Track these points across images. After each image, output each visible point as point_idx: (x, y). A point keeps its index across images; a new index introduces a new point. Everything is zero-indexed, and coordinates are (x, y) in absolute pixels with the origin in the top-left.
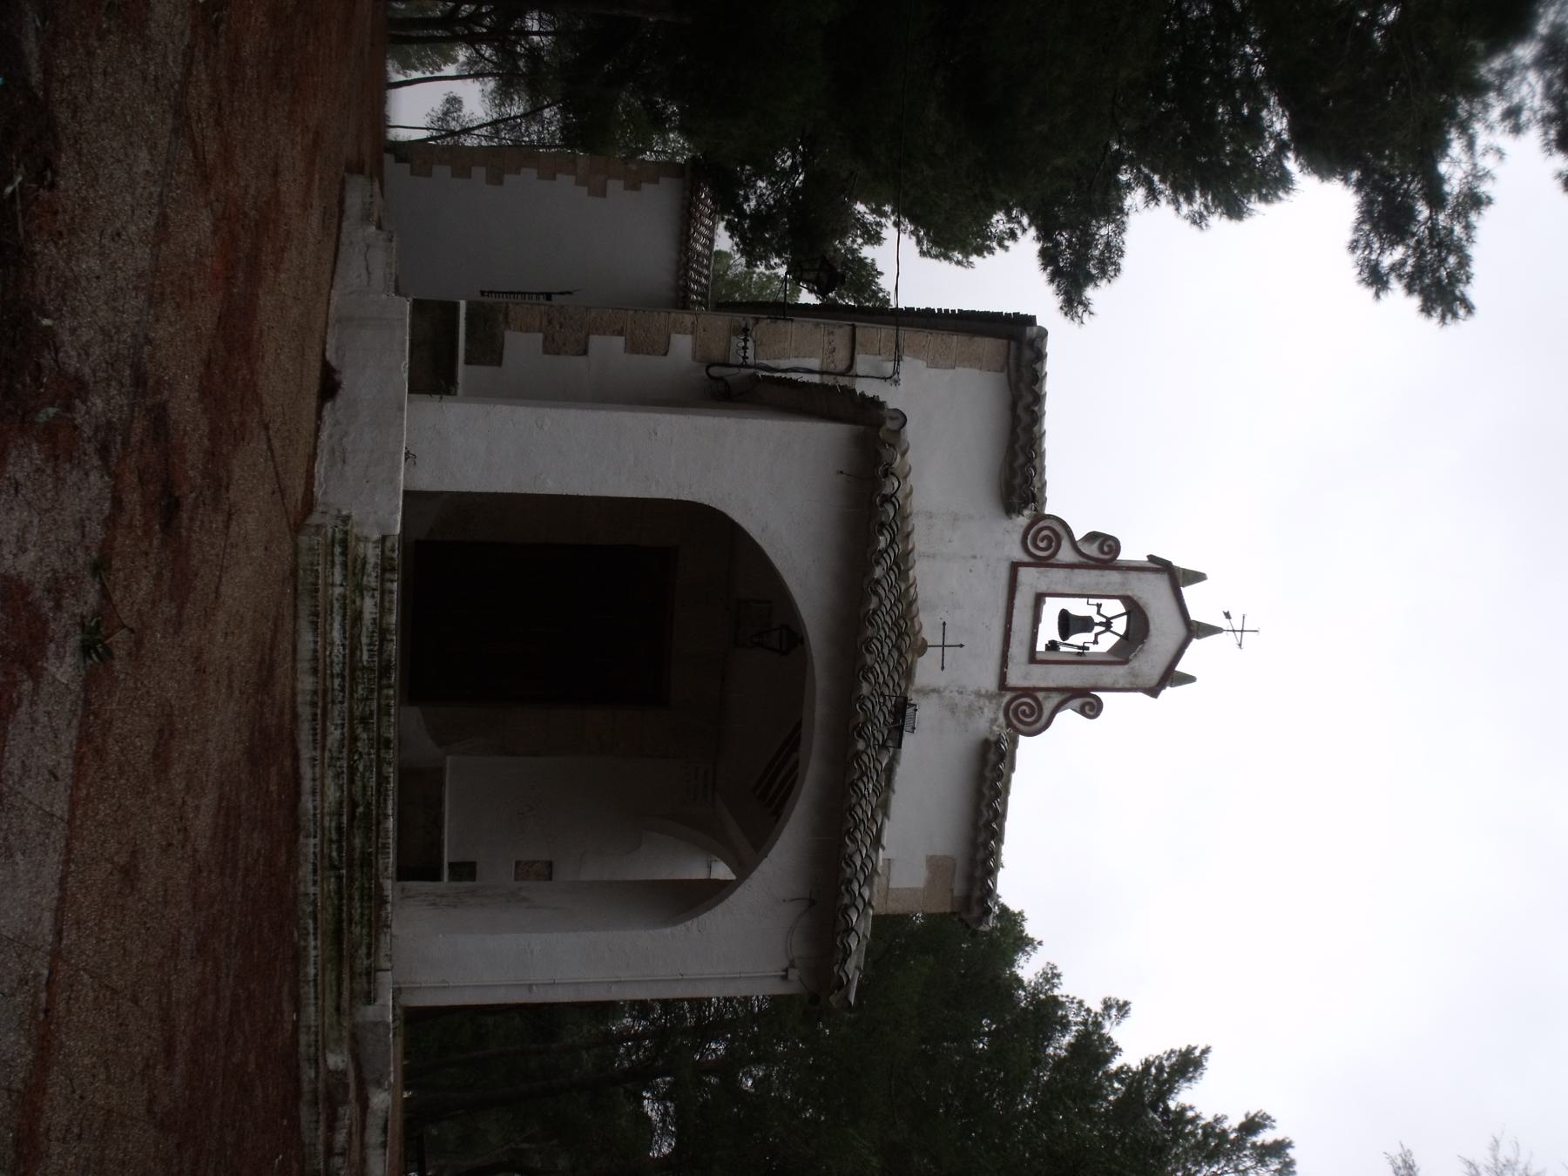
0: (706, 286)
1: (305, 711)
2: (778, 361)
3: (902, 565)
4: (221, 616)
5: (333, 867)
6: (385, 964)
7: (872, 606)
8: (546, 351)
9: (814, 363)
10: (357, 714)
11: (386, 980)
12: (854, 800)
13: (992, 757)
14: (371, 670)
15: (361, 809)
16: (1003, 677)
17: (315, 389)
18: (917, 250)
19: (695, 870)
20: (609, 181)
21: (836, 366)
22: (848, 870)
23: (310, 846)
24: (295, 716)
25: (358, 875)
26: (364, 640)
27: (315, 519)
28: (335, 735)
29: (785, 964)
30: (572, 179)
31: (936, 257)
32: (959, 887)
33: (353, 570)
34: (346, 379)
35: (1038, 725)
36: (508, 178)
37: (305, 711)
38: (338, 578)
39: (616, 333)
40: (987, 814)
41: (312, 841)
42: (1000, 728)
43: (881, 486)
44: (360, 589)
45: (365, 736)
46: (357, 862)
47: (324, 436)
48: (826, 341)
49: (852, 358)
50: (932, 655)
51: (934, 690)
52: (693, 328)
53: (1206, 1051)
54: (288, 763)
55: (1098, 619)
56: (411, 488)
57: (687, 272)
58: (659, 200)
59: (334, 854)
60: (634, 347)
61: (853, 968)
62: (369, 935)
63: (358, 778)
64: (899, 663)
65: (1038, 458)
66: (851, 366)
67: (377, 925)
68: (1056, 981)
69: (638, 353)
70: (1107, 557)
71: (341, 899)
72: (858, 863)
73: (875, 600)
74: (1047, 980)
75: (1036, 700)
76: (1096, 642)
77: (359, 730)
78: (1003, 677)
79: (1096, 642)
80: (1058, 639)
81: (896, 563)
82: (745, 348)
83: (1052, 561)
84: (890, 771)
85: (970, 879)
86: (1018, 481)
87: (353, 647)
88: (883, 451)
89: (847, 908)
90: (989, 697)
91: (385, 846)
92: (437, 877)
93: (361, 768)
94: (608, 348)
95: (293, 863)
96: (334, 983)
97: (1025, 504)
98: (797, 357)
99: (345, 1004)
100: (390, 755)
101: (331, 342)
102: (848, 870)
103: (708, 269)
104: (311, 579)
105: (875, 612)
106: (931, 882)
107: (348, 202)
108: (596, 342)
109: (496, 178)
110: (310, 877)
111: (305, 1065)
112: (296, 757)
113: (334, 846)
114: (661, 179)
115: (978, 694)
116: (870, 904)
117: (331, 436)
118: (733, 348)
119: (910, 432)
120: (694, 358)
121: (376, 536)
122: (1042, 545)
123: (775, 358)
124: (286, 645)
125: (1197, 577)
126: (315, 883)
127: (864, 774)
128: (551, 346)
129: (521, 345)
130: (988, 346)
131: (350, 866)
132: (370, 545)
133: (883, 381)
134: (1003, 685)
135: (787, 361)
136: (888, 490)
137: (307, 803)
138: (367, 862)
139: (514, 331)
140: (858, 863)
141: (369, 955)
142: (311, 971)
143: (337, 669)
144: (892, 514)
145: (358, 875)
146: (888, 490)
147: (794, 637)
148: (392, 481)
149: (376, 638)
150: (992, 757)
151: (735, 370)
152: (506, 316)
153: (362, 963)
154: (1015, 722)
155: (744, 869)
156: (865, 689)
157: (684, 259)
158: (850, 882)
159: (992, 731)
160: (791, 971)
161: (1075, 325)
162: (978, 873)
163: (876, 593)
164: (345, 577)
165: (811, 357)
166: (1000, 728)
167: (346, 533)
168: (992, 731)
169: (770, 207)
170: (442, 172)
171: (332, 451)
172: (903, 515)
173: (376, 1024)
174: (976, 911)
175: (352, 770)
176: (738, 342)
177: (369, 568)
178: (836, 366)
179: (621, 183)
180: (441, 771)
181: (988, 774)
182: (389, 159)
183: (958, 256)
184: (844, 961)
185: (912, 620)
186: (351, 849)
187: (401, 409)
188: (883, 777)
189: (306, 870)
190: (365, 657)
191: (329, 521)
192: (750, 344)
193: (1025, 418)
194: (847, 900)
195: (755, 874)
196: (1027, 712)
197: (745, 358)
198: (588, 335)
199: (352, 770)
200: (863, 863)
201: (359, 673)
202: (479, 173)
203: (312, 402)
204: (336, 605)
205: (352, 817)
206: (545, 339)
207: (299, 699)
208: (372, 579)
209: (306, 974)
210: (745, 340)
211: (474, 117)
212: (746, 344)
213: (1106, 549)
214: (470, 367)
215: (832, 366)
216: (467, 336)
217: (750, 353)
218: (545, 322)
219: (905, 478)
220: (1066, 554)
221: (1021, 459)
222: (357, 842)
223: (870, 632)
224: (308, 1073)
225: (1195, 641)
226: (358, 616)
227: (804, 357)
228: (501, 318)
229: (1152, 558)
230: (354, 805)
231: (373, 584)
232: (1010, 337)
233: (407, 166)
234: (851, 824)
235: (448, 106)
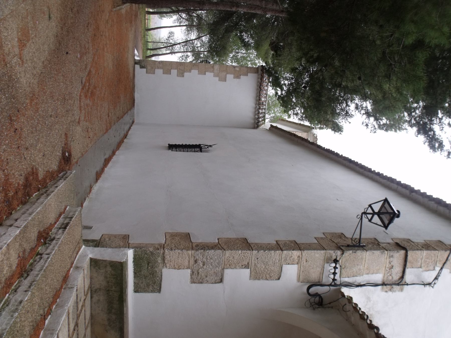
2: (355, 278)
20: (227, 75)
21: (392, 278)
30: (212, 74)
36: (186, 74)
39: (244, 267)
48: (388, 263)
49: (404, 272)
52: (299, 260)
60: (255, 276)
66: (402, 277)
69: (259, 279)
82: (334, 274)
98: (368, 274)
108: (229, 273)
109: (181, 74)
114: (249, 74)
118: (326, 273)
120: (298, 280)
123: (353, 276)
133: (423, 286)
135: (362, 277)
139: (169, 268)
151: (327, 288)
152: (164, 259)
161: (400, 132)
165: (377, 273)
170: (159, 72)
176: (330, 267)
178: (392, 278)
179: (232, 76)
182: (137, 67)
192: (337, 271)
198: (223, 269)
202: (174, 72)
206: (193, 273)
210: (335, 268)
211: (178, 38)
212: (335, 271)
214: (137, 294)
215: (390, 278)
216: (135, 273)
218: (192, 262)
227: (373, 274)
228: (159, 260)
235: (169, 35)
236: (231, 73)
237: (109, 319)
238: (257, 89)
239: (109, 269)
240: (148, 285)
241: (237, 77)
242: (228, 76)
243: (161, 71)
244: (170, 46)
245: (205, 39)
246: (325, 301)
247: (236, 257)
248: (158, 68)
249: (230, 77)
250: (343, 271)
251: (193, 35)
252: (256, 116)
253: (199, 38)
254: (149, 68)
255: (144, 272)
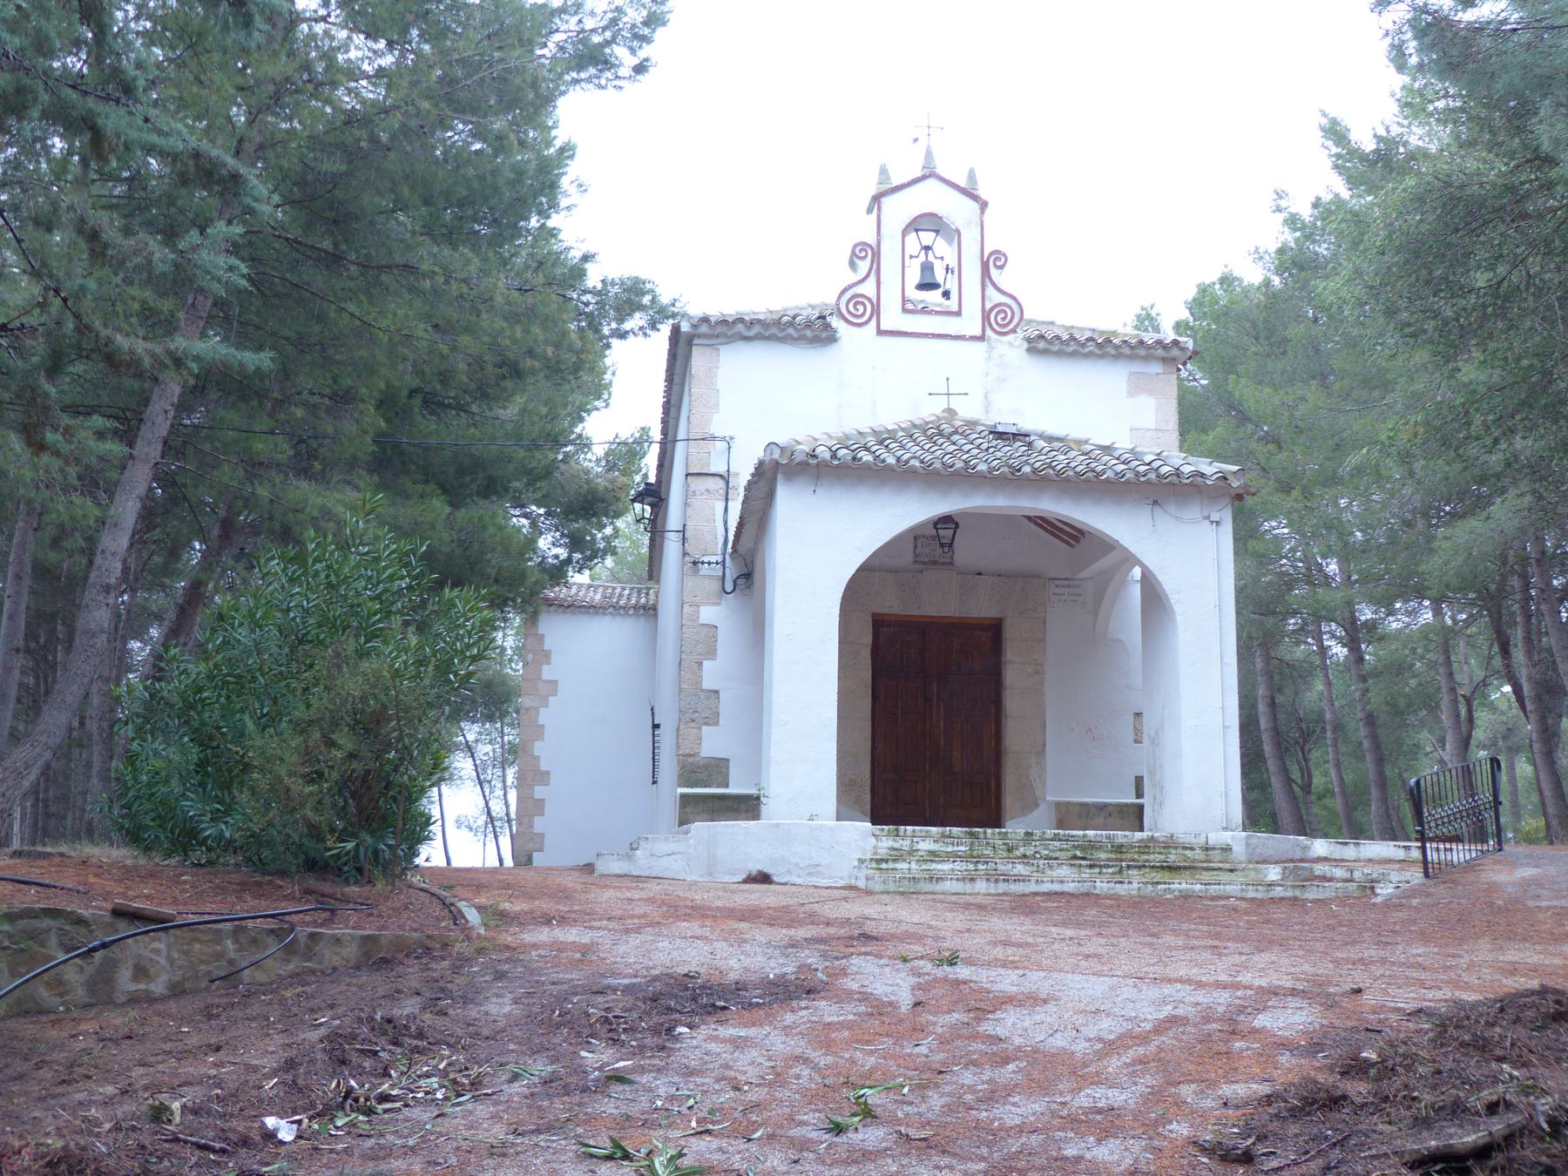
0: (632, 589)
1: (1002, 887)
3: (884, 438)
4: (933, 923)
5: (1120, 872)
6: (1202, 840)
7: (918, 464)
8: (717, 723)
9: (720, 506)
10: (1005, 854)
11: (1218, 838)
12: (1071, 473)
13: (1042, 345)
14: (972, 844)
15: (1078, 853)
16: (973, 338)
17: (765, 887)
18: (603, 411)
19: (1136, 592)
20: (544, 678)
22: (1128, 476)
23: (1102, 886)
24: (1005, 894)
25: (1129, 856)
26: (950, 849)
27: (861, 884)
28: (1020, 869)
29: (1207, 523)
31: (610, 394)
32: (1155, 368)
33: (897, 856)
34: (755, 867)
35: (1015, 306)
37: (1002, 887)
38: (904, 866)
40: (1091, 347)
41: (1098, 884)
42: (1017, 339)
43: (824, 460)
44: (912, 852)
45: (1022, 849)
46: (1119, 856)
47: (799, 881)
49: (714, 475)
50: (956, 403)
51: (986, 397)
53: (1325, 115)
54: (1039, 898)
55: (922, 258)
56: (834, 814)
57: (621, 607)
58: (557, 632)
59: (1110, 870)
61: (1209, 468)
62: (1176, 848)
63: (1054, 855)
64: (962, 434)
65: (789, 313)
66: (721, 476)
67: (1170, 844)
68: (1261, 251)
70: (870, 253)
71: (1145, 866)
72: (1123, 467)
73: (913, 462)
74: (1261, 258)
75: (992, 309)
76: (942, 258)
77: (1018, 853)
78: (973, 338)
79: (942, 258)
80: (940, 291)
81: (881, 443)
82: (709, 563)
83: (875, 301)
84: (1051, 439)
85: (1147, 359)
86: (809, 333)
87: (955, 856)
88: (797, 460)
89: (1158, 476)
90: (991, 349)
91: (1108, 837)
92: (1141, 808)
93: (1046, 852)
94: (712, 674)
95: (1116, 898)
96: (1211, 873)
97: (828, 326)
99: (1227, 866)
100: (1038, 832)
101: (727, 879)
102: (1128, 476)
103: (614, 589)
104: (906, 882)
105: (922, 462)
106: (1150, 392)
107: (618, 871)
108: (708, 683)
109: (544, 777)
110: (1125, 886)
111: (1272, 894)
112: (1036, 894)
113: (1104, 870)
114: (540, 632)
115: (989, 359)
116: (1159, 454)
117: (799, 876)
118: (711, 573)
119: (782, 439)
120: (719, 604)
121: (873, 840)
122: (861, 308)
124: (954, 898)
125: (884, 171)
126: (1130, 883)
127: (1050, 466)
128: (713, 719)
129: (712, 744)
130: (699, 360)
131: (1121, 860)
132: (880, 844)
134: (982, 338)
136: (827, 455)
137: (1070, 887)
138: (1119, 849)
140: (1123, 467)
141: (1192, 849)
142: (1198, 887)
143: (971, 867)
144: (845, 451)
145: (1129, 856)
146: (827, 455)
147: (946, 520)
148: (832, 829)
149: (948, 840)
150: (1042, 345)
151: (727, 570)
153: (1198, 854)
154: (1011, 326)
155: (1130, 559)
156: (982, 467)
157: (611, 610)
158: (1137, 474)
159: (1020, 346)
160: (1212, 519)
162: (1142, 352)
163: (907, 462)
164: (904, 860)
166: (1017, 339)
167: (871, 860)
168: (1020, 346)
169: (563, 535)
170: (539, 824)
171: (810, 874)
172: (844, 442)
173: (1248, 845)
174: (1175, 352)
175: (1048, 858)
177: (896, 845)
179: (545, 668)
180: (1058, 805)
181: (1056, 348)
183: (607, 377)
184: (1203, 475)
185: (927, 423)
186: (1109, 860)
187: (777, 825)
188: (1056, 445)
189: (1121, 889)
190: (963, 848)
191: (865, 872)
192: (706, 559)
193: (756, 329)
194: (1153, 476)
195: (1132, 549)
196: (1002, 315)
197: (717, 563)
199: (1048, 858)
200: (1123, 463)
201: (975, 853)
202: (539, 792)
203: (772, 887)
204: (924, 867)
205: (1084, 858)
206: (706, 724)
207: (993, 891)
208: (905, 843)
209: (1201, 891)
210: (703, 563)
213: (863, 254)
217: (713, 559)
218: (693, 725)
219: (816, 440)
220: (868, 289)
221: (791, 331)
222: (1103, 856)
223: (938, 465)
224: (1278, 892)
225: (938, 171)
226: (932, 853)
228: (691, 760)
229: (869, 211)
230: (1075, 857)
231: (909, 842)
232: (690, 343)
233: (535, 855)
234: (1090, 474)
236: (540, 672)
237: (746, 812)
238: (573, 613)
239: (688, 809)
240: (720, 772)
241: (546, 656)
242: (545, 676)
243: (537, 820)
244: (494, 827)
245: (471, 732)
246: (746, 571)
247: (688, 676)
248: (532, 826)
249: (547, 672)
250: (710, 551)
251: (462, 764)
252: (631, 612)
253: (470, 749)
254: (531, 846)
255: (704, 776)
